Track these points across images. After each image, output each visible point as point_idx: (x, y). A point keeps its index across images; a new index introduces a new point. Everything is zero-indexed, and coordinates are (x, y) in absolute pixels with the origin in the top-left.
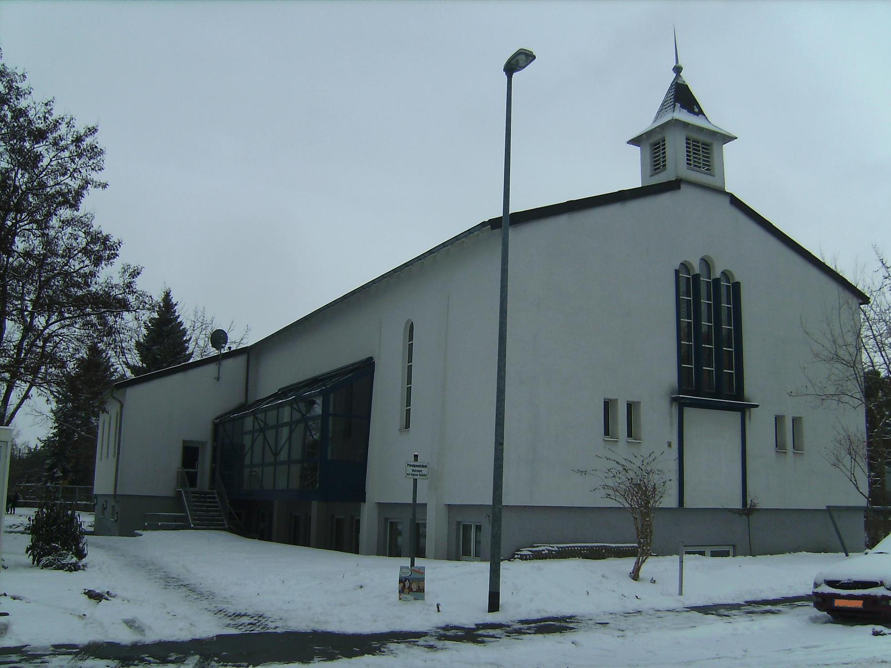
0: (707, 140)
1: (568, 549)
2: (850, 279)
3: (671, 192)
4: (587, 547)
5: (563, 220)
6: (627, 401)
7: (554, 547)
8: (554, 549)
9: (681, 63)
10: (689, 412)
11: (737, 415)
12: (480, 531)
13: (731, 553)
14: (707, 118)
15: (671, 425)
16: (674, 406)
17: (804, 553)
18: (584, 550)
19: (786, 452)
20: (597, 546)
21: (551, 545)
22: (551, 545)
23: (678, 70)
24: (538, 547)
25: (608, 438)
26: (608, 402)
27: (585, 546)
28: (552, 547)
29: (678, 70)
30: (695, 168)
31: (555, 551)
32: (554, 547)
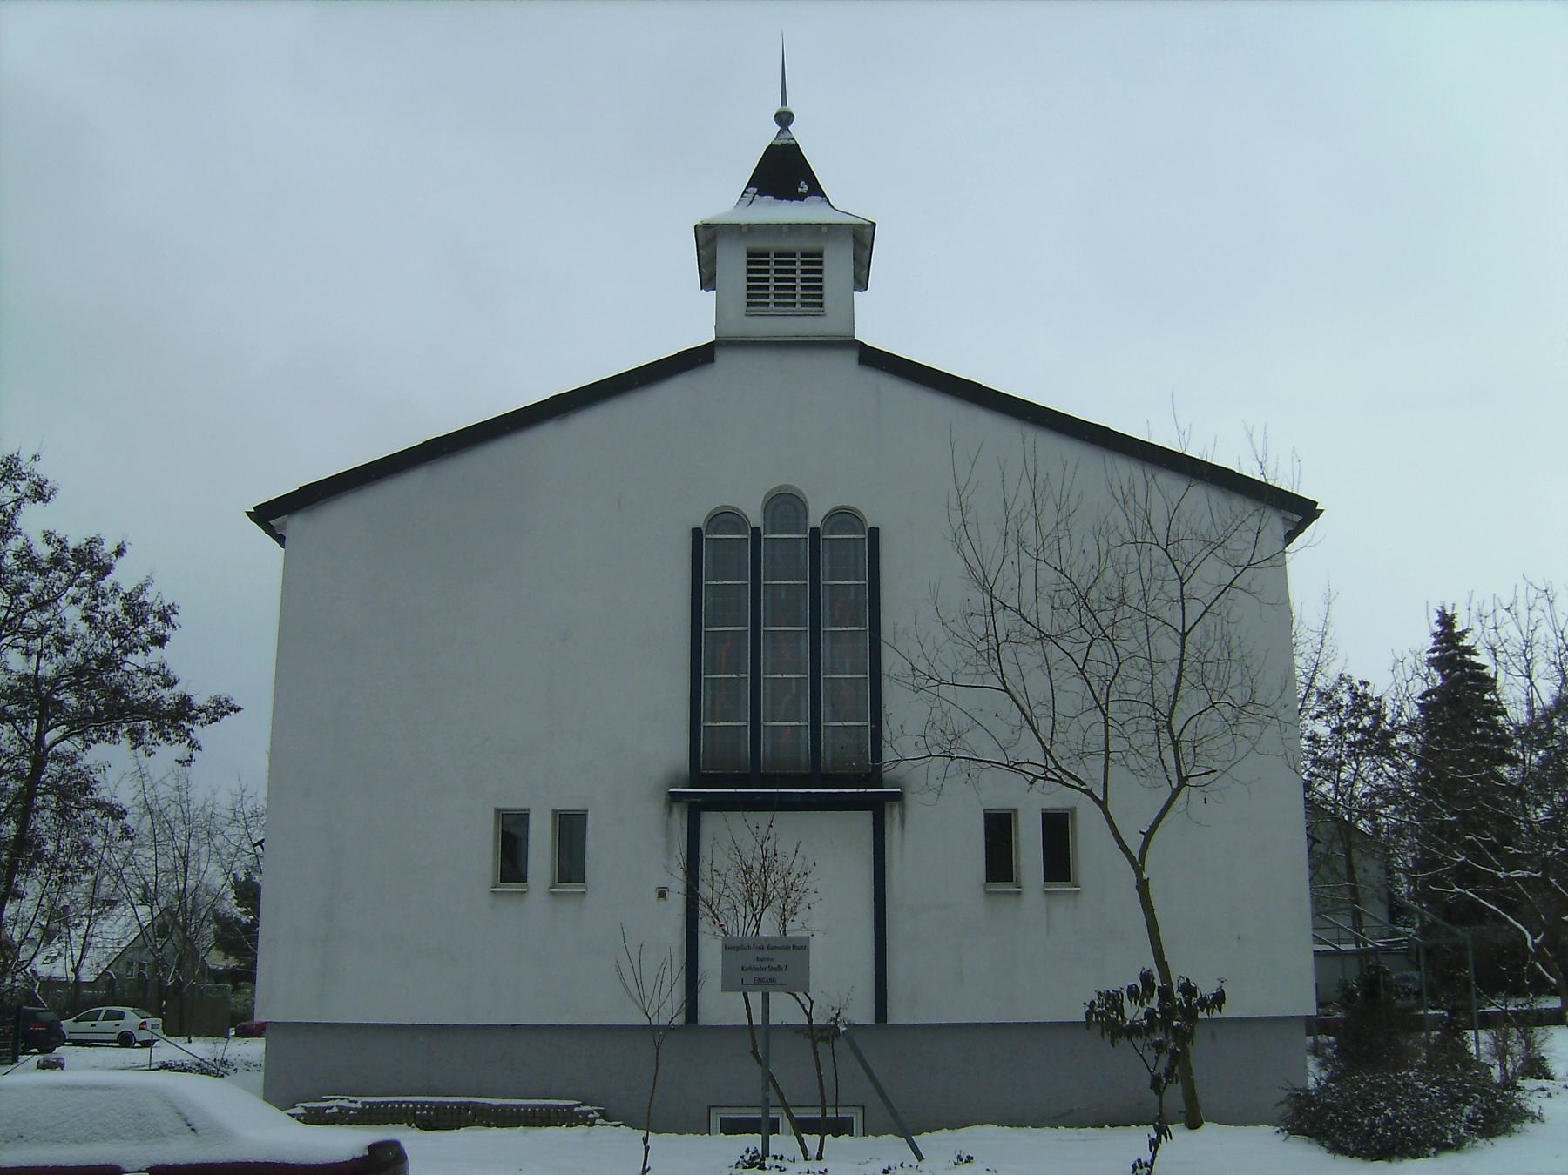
0: (810, 245)
1: (408, 1107)
2: (1250, 470)
3: (691, 371)
4: (432, 1103)
5: (417, 479)
6: (1042, 810)
7: (356, 1102)
8: (353, 1105)
9: (792, 106)
10: (712, 823)
11: (864, 819)
12: (38, 1062)
13: (858, 1125)
14: (828, 200)
15: (668, 850)
16: (676, 814)
17: (990, 1129)
18: (423, 1109)
19: (1019, 893)
20: (455, 1103)
21: (352, 1098)
22: (352, 1098)
23: (784, 119)
24: (327, 1100)
25: (1068, 886)
26: (1011, 814)
27: (426, 1102)
28: (351, 1102)
29: (784, 119)
30: (777, 308)
31: (355, 1110)
32: (356, 1102)
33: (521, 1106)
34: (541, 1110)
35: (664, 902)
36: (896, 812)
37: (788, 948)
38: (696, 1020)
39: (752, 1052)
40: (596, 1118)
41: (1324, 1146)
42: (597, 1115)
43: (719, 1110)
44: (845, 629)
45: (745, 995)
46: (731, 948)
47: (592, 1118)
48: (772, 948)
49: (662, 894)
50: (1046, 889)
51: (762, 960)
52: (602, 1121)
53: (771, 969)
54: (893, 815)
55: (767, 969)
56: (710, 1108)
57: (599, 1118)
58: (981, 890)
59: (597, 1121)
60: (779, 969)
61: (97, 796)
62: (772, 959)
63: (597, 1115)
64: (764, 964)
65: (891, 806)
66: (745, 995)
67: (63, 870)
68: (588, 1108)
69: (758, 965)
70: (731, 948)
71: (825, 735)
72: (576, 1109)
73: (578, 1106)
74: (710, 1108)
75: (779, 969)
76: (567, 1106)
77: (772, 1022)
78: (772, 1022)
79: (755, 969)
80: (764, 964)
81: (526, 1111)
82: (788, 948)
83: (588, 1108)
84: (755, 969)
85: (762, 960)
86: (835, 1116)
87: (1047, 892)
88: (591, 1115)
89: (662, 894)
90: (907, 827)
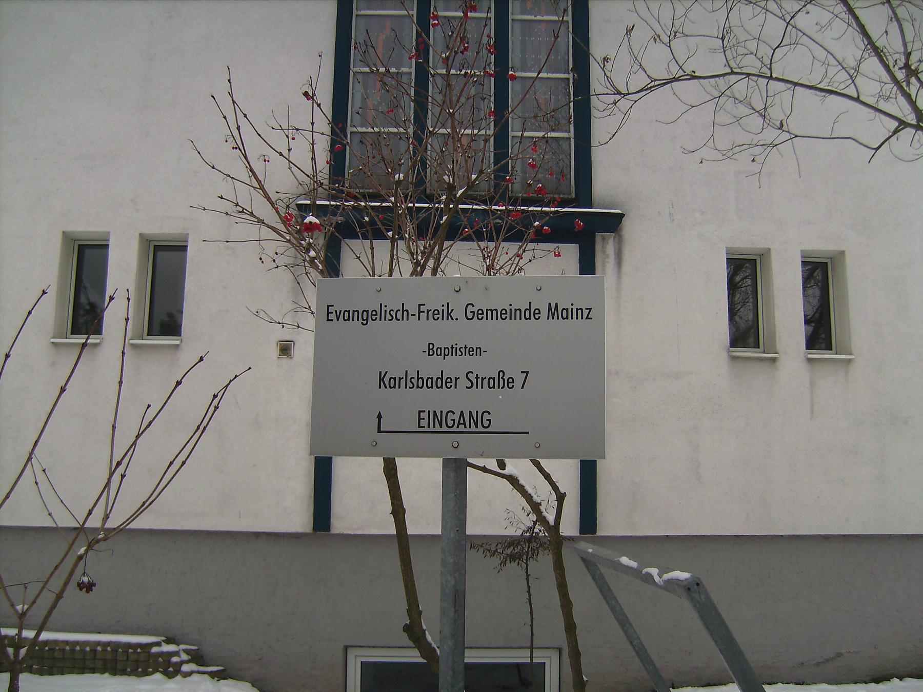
19: (774, 360)
33: (77, 643)
34: (104, 650)
35: (289, 361)
36: (610, 248)
37: (531, 313)
38: (594, 531)
39: (407, 629)
40: (182, 662)
41: (600, 573)
42: (185, 657)
43: (359, 652)
44: (539, 18)
45: (390, 470)
46: (346, 315)
47: (176, 663)
48: (479, 314)
49: (285, 350)
50: (810, 356)
51: (445, 353)
52: (192, 667)
53: (475, 382)
54: (605, 248)
55: (463, 382)
56: (346, 648)
57: (187, 662)
58: (724, 355)
59: (185, 668)
60: (502, 381)
61: (508, 562)
62: (479, 351)
63: (185, 657)
64: (454, 366)
65: (604, 239)
66: (390, 470)
67: (482, 546)
68: (171, 648)
69: (432, 367)
70: (346, 315)
71: (513, 148)
72: (155, 650)
73: (158, 644)
74: (346, 648)
75: (502, 381)
76: (140, 645)
77: (472, 529)
78: (472, 529)
79: (421, 382)
80: (454, 366)
81: (83, 651)
82: (531, 313)
83: (171, 648)
84: (421, 382)
85: (445, 353)
86: (528, 660)
87: (810, 360)
88: (175, 659)
89: (285, 350)
90: (626, 268)
